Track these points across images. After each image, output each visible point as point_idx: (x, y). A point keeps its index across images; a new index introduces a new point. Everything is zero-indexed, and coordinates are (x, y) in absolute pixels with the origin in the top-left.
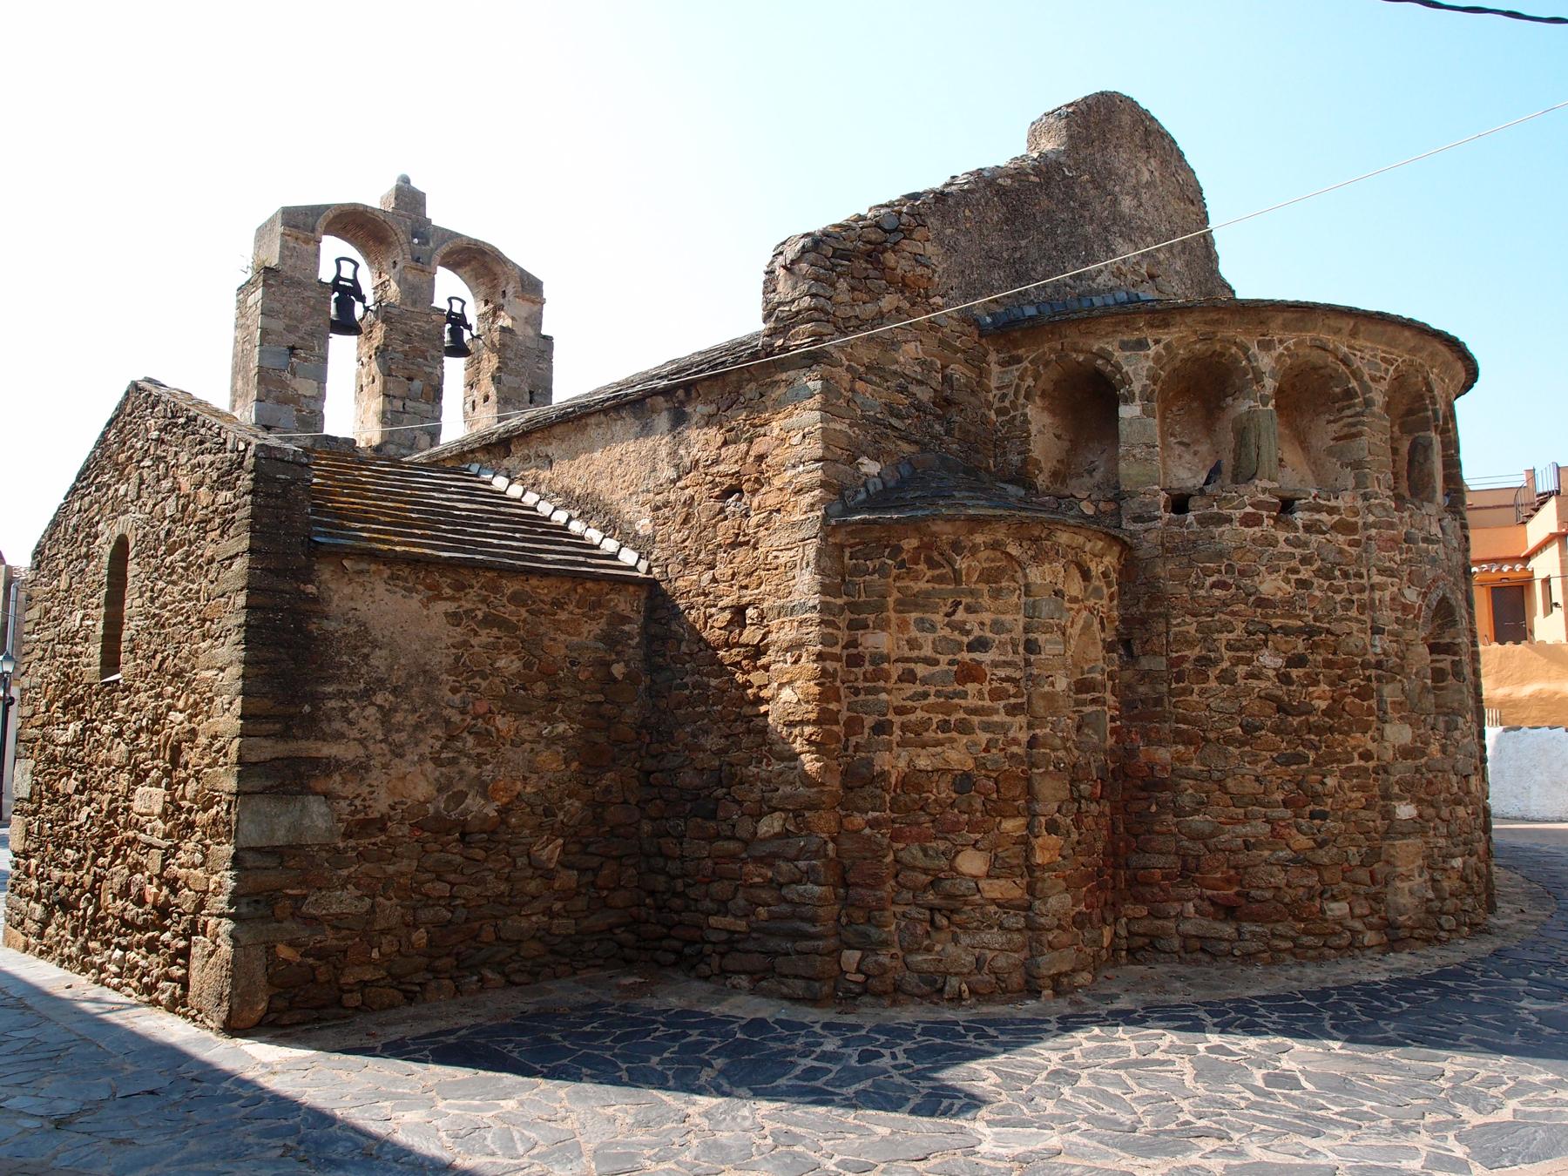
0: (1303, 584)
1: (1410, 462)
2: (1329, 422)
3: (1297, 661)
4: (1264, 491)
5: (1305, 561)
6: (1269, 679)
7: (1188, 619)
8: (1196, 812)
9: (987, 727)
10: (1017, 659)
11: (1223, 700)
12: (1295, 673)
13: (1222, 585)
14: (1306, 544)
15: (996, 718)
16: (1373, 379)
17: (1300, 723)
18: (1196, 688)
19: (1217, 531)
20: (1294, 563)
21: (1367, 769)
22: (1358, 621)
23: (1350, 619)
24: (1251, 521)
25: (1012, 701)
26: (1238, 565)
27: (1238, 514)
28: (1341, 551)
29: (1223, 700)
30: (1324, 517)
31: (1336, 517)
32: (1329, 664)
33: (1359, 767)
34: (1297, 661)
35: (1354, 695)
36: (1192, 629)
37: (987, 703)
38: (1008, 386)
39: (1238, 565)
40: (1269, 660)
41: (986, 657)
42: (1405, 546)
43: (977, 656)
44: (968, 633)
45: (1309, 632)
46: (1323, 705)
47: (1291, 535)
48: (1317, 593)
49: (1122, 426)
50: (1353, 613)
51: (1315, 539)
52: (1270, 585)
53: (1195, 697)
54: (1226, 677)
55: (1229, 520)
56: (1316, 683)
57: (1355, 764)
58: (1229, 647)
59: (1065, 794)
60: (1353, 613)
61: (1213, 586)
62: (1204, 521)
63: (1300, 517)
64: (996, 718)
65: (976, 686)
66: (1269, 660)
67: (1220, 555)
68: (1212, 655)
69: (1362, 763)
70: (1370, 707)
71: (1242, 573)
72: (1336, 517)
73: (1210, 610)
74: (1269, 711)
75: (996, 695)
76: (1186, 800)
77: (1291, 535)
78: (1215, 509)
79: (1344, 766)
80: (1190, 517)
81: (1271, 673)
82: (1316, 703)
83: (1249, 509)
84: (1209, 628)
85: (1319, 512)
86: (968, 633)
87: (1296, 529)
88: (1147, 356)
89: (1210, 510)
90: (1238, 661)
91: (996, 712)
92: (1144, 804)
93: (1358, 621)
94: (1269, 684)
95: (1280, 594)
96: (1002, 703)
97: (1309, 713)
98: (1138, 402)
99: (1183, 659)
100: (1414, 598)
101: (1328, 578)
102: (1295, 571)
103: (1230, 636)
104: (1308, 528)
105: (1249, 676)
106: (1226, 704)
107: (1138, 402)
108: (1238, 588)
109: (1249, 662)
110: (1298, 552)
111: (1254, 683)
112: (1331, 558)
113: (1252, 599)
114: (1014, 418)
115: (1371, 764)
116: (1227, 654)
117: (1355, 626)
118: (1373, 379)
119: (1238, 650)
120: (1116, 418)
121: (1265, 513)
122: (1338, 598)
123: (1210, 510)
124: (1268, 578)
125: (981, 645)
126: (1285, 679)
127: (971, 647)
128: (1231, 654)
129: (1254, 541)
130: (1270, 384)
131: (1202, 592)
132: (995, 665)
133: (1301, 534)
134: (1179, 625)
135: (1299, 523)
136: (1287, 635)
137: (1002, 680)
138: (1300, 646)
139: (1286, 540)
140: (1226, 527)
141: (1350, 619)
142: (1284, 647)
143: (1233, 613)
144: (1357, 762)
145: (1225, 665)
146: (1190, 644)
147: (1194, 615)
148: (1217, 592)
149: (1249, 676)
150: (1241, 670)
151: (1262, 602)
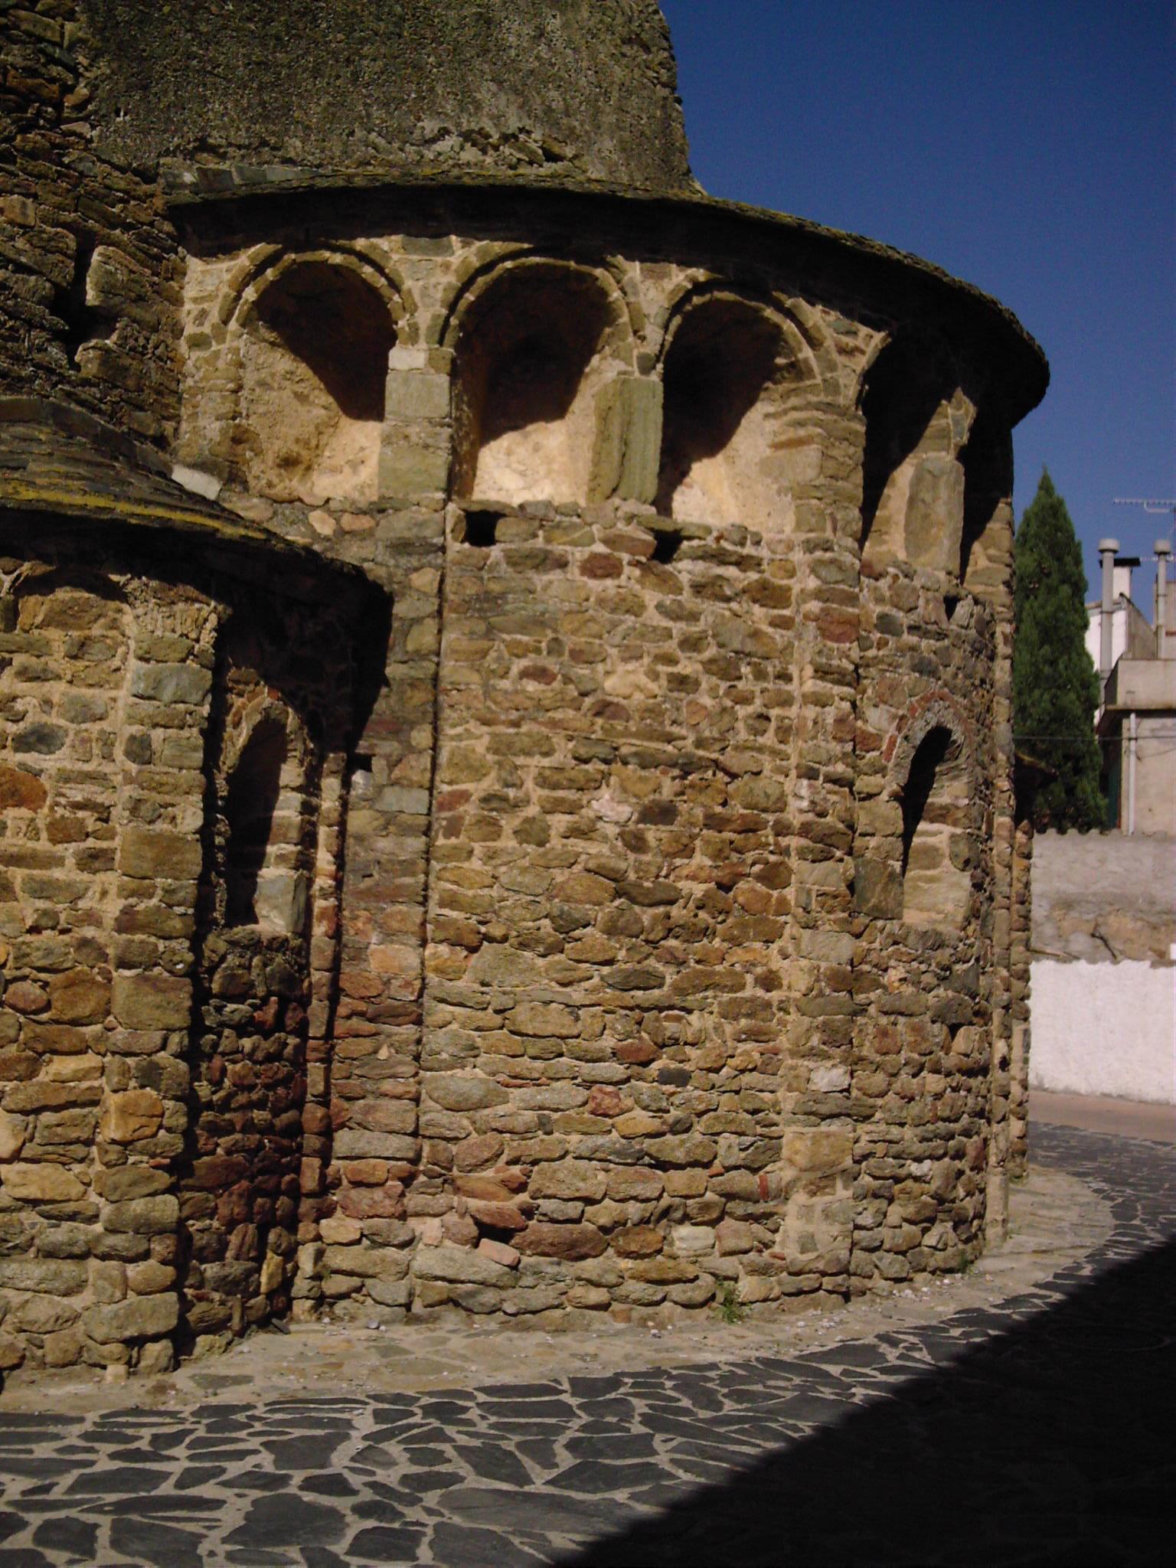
0: (681, 682)
1: (912, 501)
2: (767, 416)
3: (662, 813)
4: (630, 518)
5: (692, 644)
6: (605, 839)
7: (473, 726)
8: (457, 1062)
9: (41, 890)
10: (107, 768)
11: (524, 871)
12: (653, 834)
13: (540, 674)
14: (694, 617)
15: (57, 874)
16: (843, 351)
17: (655, 919)
18: (478, 848)
19: (540, 579)
20: (671, 646)
21: (768, 1005)
22: (774, 753)
23: (760, 749)
24: (601, 568)
25: (91, 842)
26: (570, 642)
27: (579, 554)
28: (756, 634)
29: (524, 871)
30: (732, 571)
31: (753, 576)
32: (714, 822)
33: (752, 1000)
34: (662, 813)
35: (759, 878)
36: (480, 746)
37: (43, 845)
38: (210, 298)
39: (570, 642)
40: (610, 806)
41: (49, 763)
42: (876, 636)
43: (31, 758)
44: (18, 718)
45: (686, 767)
46: (699, 889)
47: (668, 600)
48: (707, 701)
49: (392, 383)
50: (769, 739)
51: (711, 610)
52: (625, 680)
53: (475, 864)
54: (533, 834)
55: (562, 564)
56: (687, 851)
57: (747, 993)
58: (543, 781)
59: (180, 1019)
60: (769, 739)
61: (525, 674)
62: (515, 561)
63: (685, 569)
64: (57, 874)
65: (24, 812)
66: (610, 806)
67: (539, 622)
68: (511, 793)
69: (760, 992)
70: (782, 901)
71: (577, 655)
72: (753, 576)
73: (514, 715)
74: (598, 894)
75: (61, 832)
76: (437, 1041)
77: (668, 600)
78: (539, 542)
79: (726, 997)
80: (495, 552)
81: (612, 830)
82: (684, 885)
83: (600, 548)
84: (510, 746)
85: (723, 563)
86: (18, 718)
87: (679, 590)
88: (446, 267)
89: (530, 544)
90: (554, 807)
91: (59, 862)
92: (367, 1044)
93: (774, 753)
94: (605, 849)
95: (638, 697)
96: (72, 847)
97: (671, 902)
98: (422, 344)
99: (465, 796)
100: (884, 724)
101: (724, 675)
102: (671, 661)
103: (546, 762)
104: (698, 589)
105: (574, 832)
106: (527, 879)
107: (422, 344)
108: (567, 680)
109: (573, 809)
110: (678, 628)
111: (578, 844)
112: (737, 646)
113: (588, 701)
114: (217, 355)
115: (775, 996)
116: (538, 793)
117: (767, 764)
118: (843, 351)
119: (555, 786)
120: (383, 368)
121: (626, 557)
122: (742, 711)
123: (530, 544)
124: (621, 668)
125: (41, 739)
126: (636, 843)
127: (23, 743)
128: (546, 792)
129: (601, 602)
130: (655, 337)
131: (505, 684)
132: (65, 777)
133: (686, 596)
134: (458, 737)
135: (684, 579)
136: (644, 767)
137: (77, 806)
138: (668, 788)
139: (659, 607)
140: (556, 575)
141: (760, 749)
142: (639, 788)
143: (554, 724)
144: (751, 991)
145: (532, 810)
146: (478, 772)
147: (486, 723)
148: (531, 686)
149: (574, 832)
150: (560, 822)
151: (604, 709)
